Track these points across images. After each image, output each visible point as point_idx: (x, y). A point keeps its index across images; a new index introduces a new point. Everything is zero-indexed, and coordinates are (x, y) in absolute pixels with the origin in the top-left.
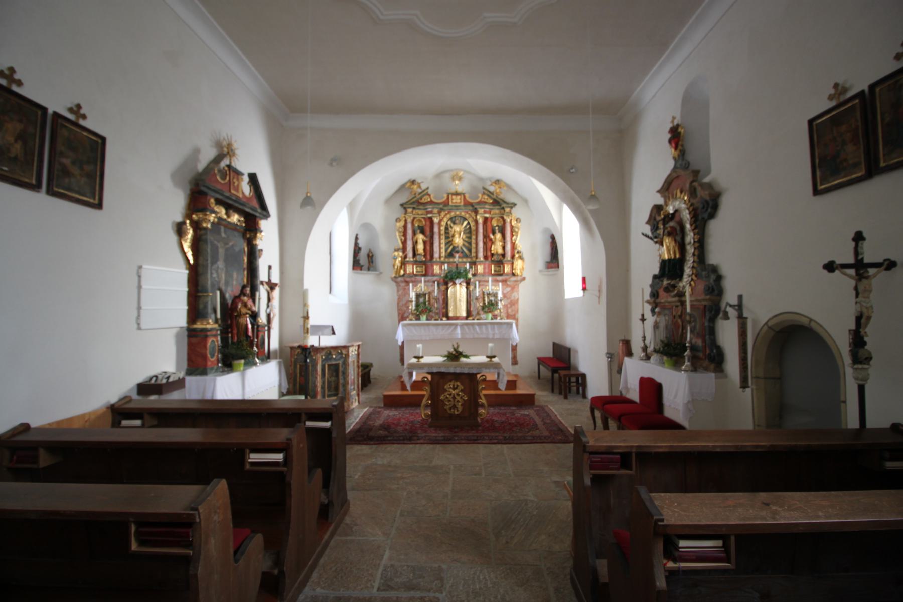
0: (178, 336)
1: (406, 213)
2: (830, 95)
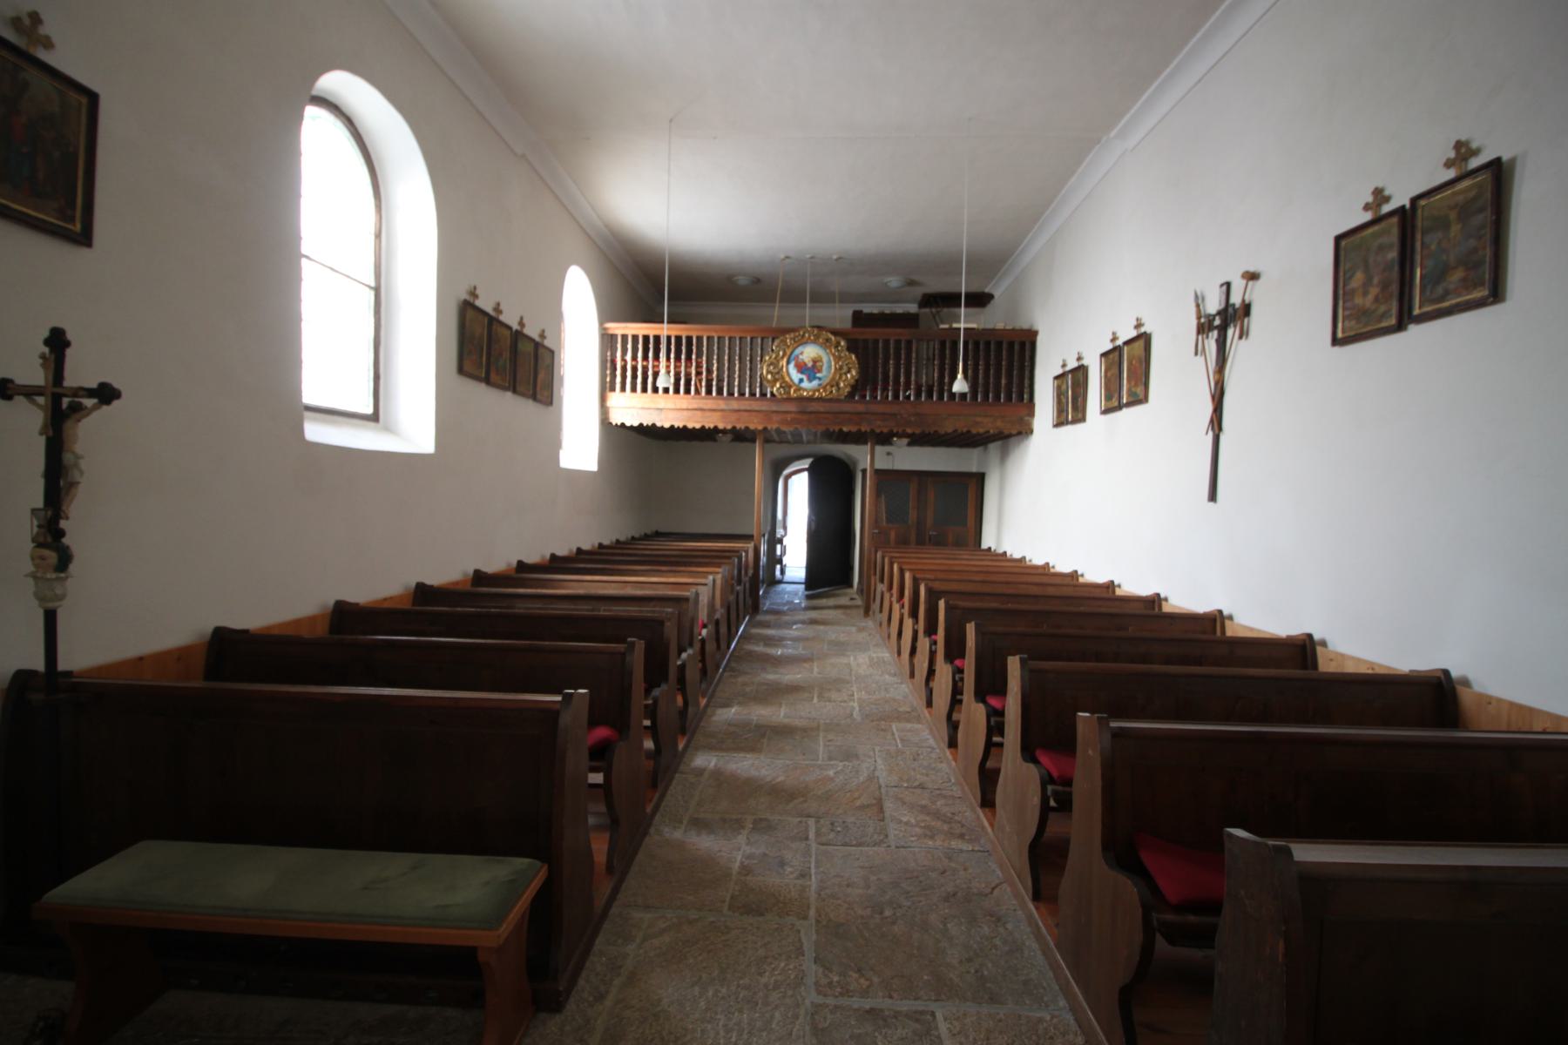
2: (1448, 160)
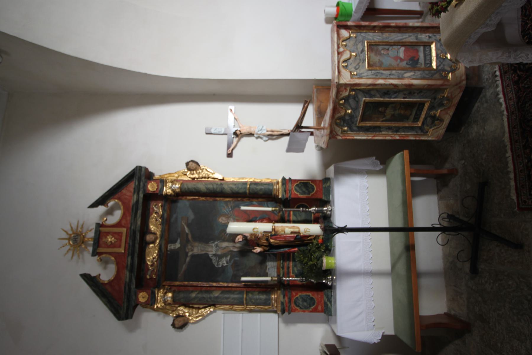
0: (287, 322)
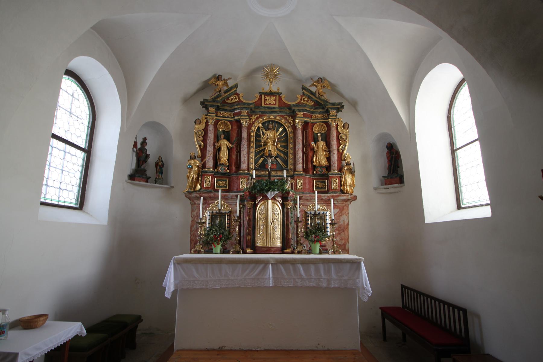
1: (208, 112)
